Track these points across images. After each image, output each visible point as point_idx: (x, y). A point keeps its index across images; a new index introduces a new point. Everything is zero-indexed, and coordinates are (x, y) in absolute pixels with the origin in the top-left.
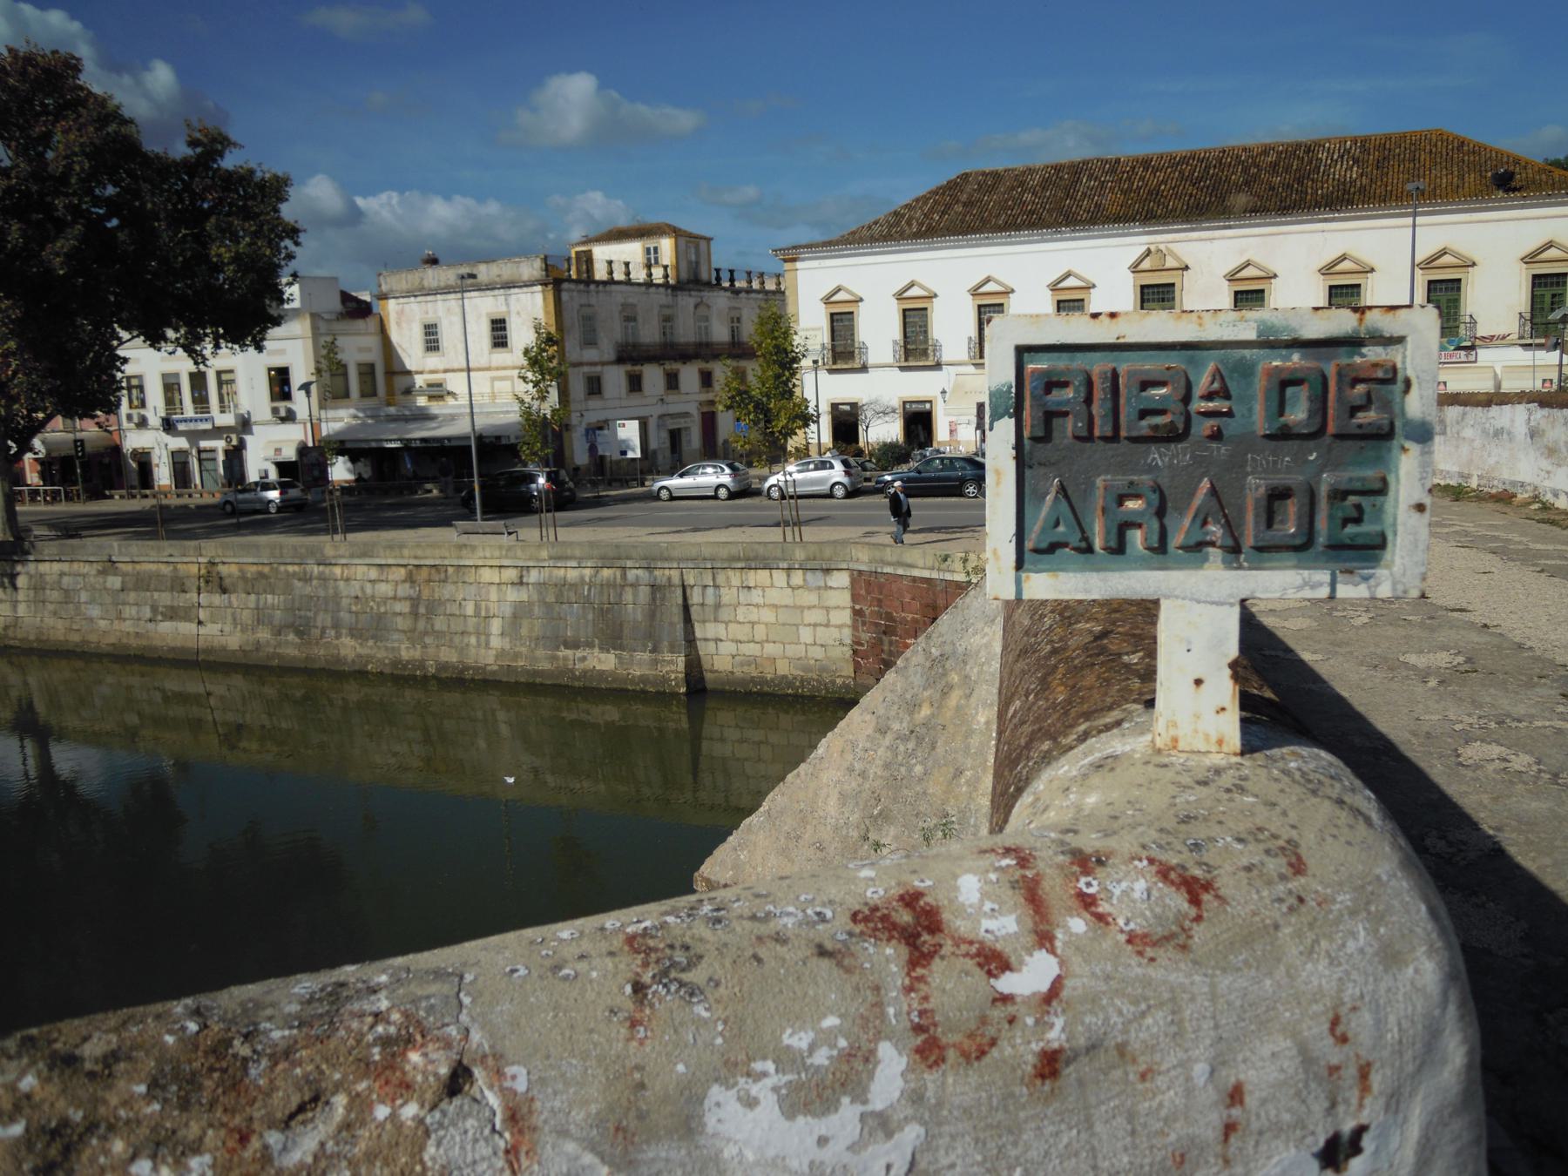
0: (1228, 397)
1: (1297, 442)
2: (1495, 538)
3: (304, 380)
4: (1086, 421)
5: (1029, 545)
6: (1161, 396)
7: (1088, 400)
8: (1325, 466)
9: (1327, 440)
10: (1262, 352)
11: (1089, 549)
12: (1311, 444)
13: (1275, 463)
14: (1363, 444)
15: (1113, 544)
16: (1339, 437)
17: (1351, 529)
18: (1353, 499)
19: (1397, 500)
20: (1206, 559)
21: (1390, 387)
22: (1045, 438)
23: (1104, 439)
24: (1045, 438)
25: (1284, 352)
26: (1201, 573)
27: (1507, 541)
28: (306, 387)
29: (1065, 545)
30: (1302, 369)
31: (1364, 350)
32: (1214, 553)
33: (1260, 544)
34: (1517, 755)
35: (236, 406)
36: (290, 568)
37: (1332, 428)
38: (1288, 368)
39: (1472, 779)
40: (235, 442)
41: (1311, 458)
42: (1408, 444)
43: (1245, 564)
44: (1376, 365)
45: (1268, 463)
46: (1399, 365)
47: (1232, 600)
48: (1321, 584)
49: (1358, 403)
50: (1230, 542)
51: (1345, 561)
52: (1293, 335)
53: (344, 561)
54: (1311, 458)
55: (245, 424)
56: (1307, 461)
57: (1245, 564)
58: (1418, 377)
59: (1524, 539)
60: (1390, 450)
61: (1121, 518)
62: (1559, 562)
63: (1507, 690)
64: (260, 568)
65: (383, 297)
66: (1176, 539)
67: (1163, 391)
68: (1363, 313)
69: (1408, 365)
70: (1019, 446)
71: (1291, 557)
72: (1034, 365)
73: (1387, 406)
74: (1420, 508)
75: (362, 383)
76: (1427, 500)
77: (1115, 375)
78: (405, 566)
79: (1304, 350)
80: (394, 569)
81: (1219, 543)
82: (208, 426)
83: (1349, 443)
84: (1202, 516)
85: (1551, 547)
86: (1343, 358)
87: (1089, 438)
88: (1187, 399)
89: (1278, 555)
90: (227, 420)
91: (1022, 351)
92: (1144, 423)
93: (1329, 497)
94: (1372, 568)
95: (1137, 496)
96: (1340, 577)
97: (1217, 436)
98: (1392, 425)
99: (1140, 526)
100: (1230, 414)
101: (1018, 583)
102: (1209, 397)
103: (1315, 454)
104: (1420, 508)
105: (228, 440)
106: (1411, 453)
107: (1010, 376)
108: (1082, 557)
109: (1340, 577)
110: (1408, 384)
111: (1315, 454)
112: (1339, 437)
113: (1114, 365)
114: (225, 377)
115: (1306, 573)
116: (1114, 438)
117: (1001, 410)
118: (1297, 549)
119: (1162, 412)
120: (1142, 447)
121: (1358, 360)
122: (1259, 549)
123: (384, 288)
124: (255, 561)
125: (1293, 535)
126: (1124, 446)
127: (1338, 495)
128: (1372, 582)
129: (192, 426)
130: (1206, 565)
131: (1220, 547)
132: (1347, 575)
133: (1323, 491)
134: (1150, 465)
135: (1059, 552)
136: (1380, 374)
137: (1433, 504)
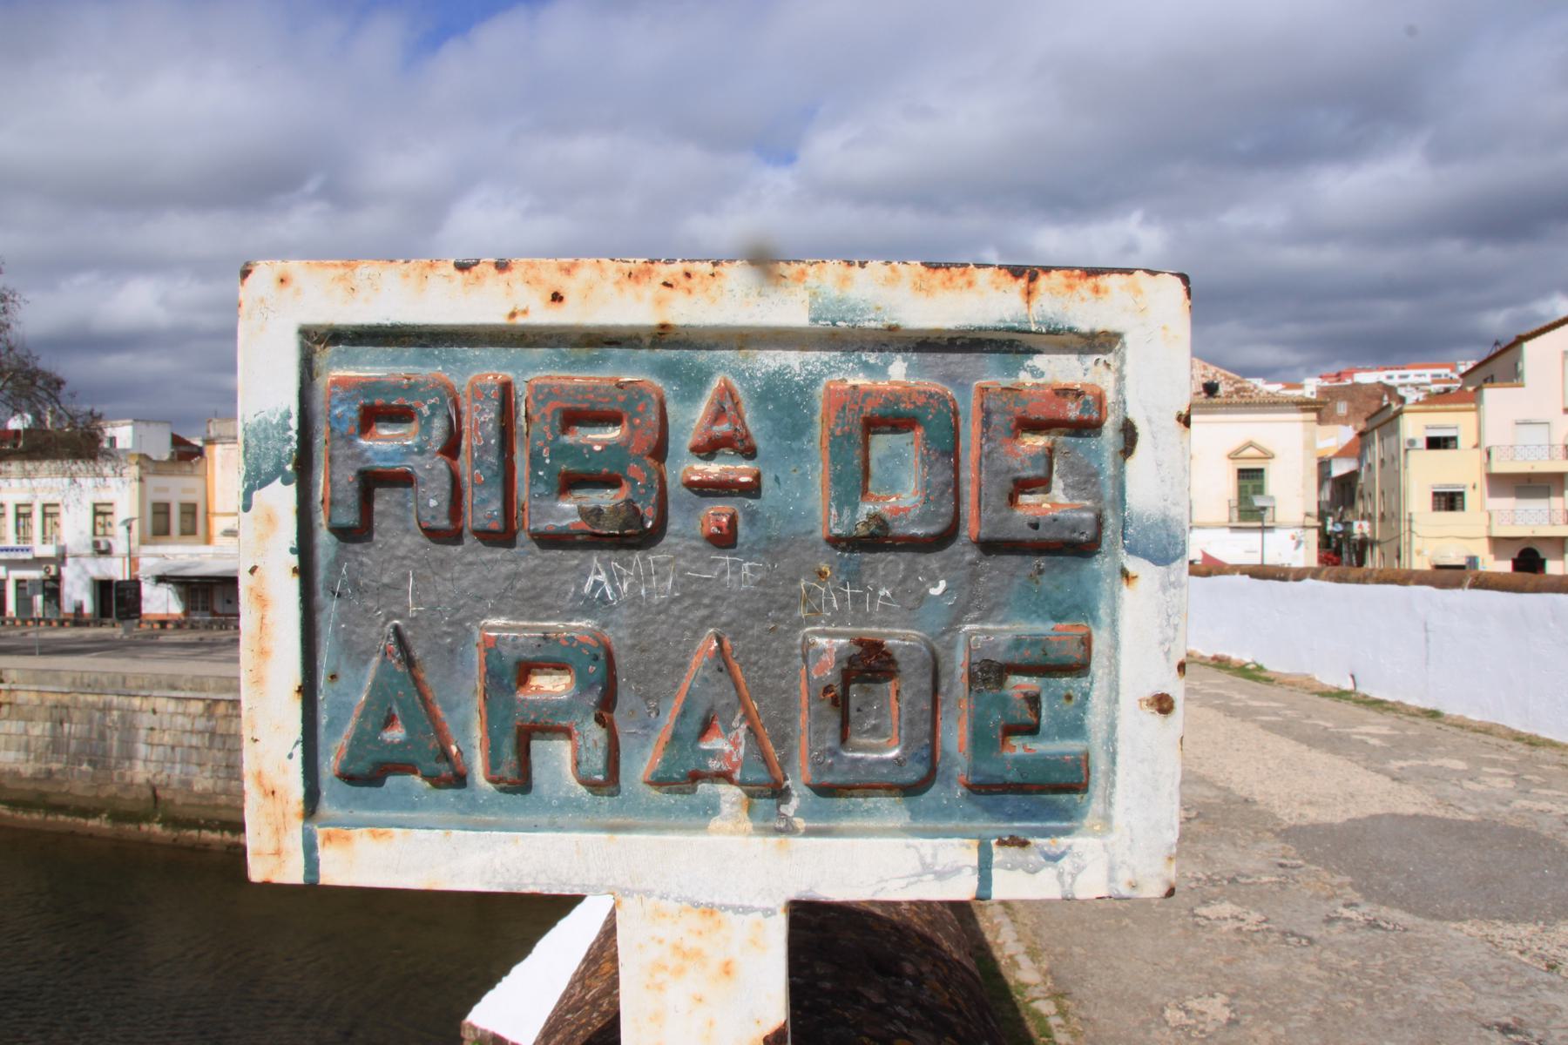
0: (750, 453)
1: (908, 556)
2: (1217, 696)
3: (127, 516)
4: (445, 495)
5: (329, 765)
6: (607, 447)
7: (451, 448)
8: (965, 610)
9: (963, 551)
10: (825, 356)
11: (459, 780)
12: (933, 561)
13: (856, 599)
14: (1042, 562)
15: (508, 770)
16: (990, 547)
17: (1019, 747)
18: (1020, 684)
19: (1114, 688)
20: (711, 808)
21: (1093, 443)
22: (356, 534)
23: (489, 538)
24: (356, 534)
25: (872, 358)
26: (699, 839)
27: (1229, 698)
28: (128, 524)
29: (407, 768)
30: (909, 392)
31: (1039, 361)
32: (730, 795)
33: (828, 779)
34: (1248, 913)
35: (58, 538)
36: (90, 698)
37: (971, 528)
38: (879, 393)
39: (1208, 940)
40: (53, 572)
41: (935, 592)
42: (1133, 564)
43: (801, 823)
44: (1064, 392)
45: (842, 600)
46: (1110, 397)
47: (769, 904)
48: (957, 870)
49: (1029, 473)
50: (758, 775)
51: (1011, 817)
52: (890, 321)
53: (144, 693)
54: (935, 592)
55: (61, 559)
56: (923, 598)
57: (801, 823)
58: (1149, 421)
59: (1243, 697)
60: (1097, 579)
61: (518, 719)
62: (1274, 719)
63: (1235, 844)
64: (60, 696)
65: (210, 441)
66: (640, 763)
67: (612, 434)
68: (1033, 278)
69: (1130, 396)
70: (305, 547)
71: (892, 811)
72: (339, 369)
73: (1086, 480)
74: (1163, 704)
75: (182, 521)
76: (1175, 688)
77: (506, 388)
78: (203, 700)
79: (915, 357)
80: (192, 702)
81: (737, 776)
82: (28, 556)
83: (1012, 561)
84: (699, 713)
85: (1265, 704)
86: (989, 373)
87: (452, 536)
88: (660, 452)
89: (871, 802)
90: (49, 551)
91: (316, 340)
92: (568, 505)
93: (972, 678)
94: (1066, 832)
95: (559, 667)
96: (999, 854)
97: (724, 540)
98: (1099, 522)
99: (567, 733)
100: (752, 489)
101: (310, 849)
102: (708, 449)
103: (943, 584)
104: (1163, 704)
105: (47, 571)
106: (1139, 585)
107: (289, 401)
108: (449, 794)
109: (999, 854)
110: (1129, 434)
111: (943, 584)
112: (990, 547)
113: (510, 375)
114: (49, 510)
115: (926, 845)
116: (502, 537)
117: (267, 467)
118: (910, 790)
119: (611, 482)
120: (573, 558)
121: (1025, 378)
122: (825, 791)
123: (213, 434)
124: (56, 689)
125: (898, 762)
126: (526, 556)
127: (990, 673)
128: (1065, 863)
129: (12, 556)
130: (716, 822)
131: (741, 784)
132: (1013, 850)
133: (959, 663)
134: (587, 599)
135: (392, 781)
136: (1073, 411)
137: (1190, 693)
